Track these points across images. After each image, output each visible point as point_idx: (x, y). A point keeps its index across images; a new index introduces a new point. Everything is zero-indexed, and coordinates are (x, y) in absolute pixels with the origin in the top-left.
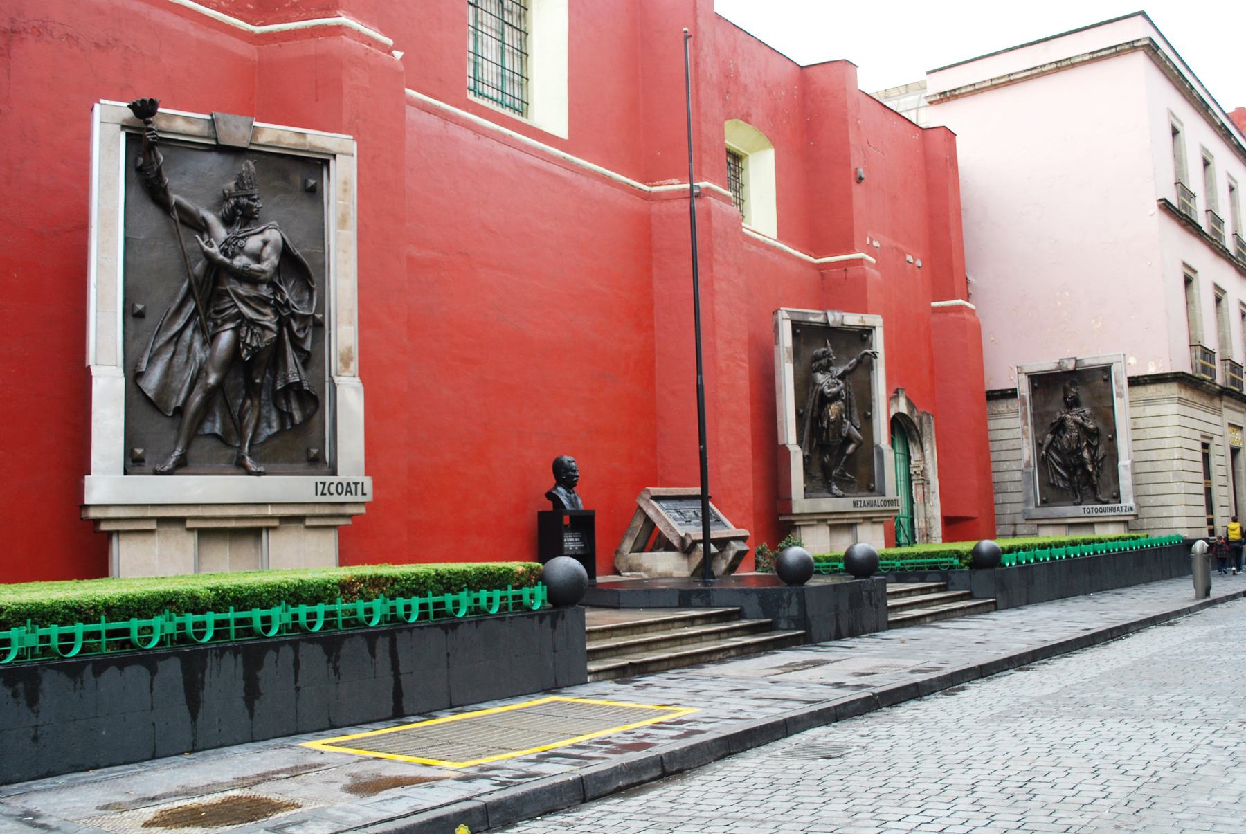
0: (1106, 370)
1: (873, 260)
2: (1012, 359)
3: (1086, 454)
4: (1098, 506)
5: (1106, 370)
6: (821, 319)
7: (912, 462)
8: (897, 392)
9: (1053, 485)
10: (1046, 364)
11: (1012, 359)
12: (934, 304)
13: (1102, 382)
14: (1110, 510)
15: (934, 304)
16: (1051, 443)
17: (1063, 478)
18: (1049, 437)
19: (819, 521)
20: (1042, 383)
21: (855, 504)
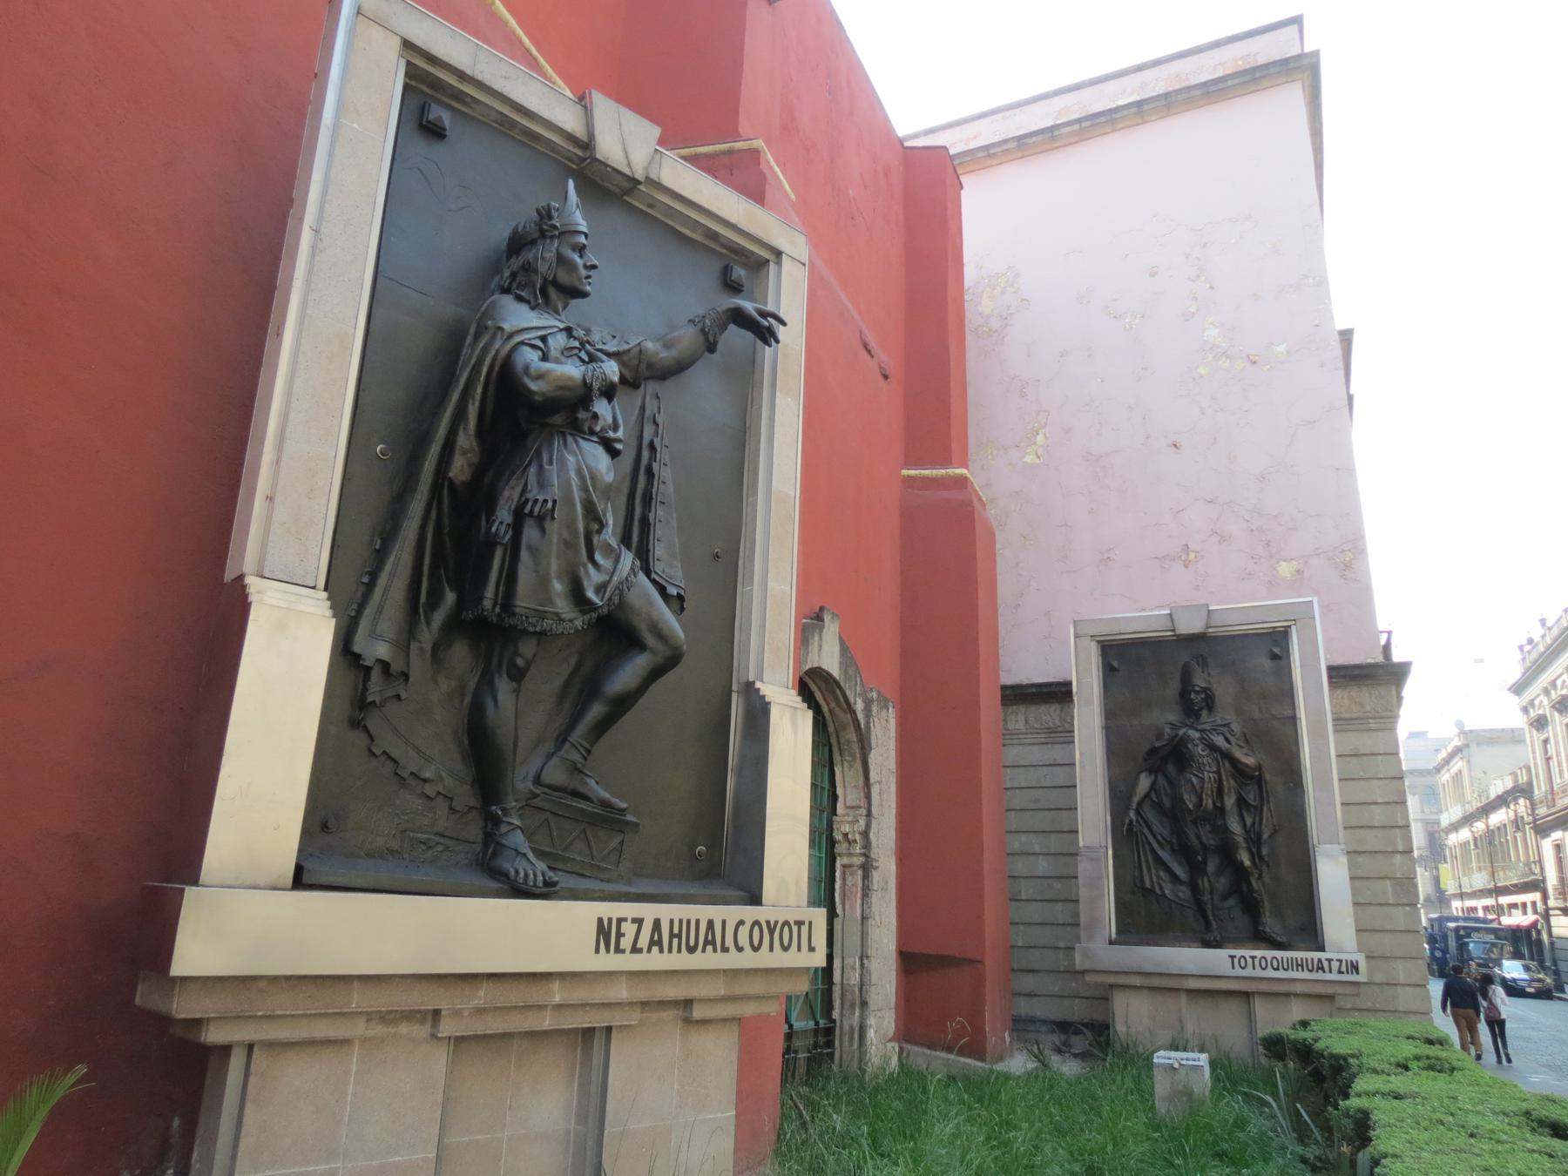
0: (1275, 643)
1: (793, 197)
2: (1048, 620)
3: (1235, 826)
4: (1269, 954)
5: (1275, 643)
6: (567, 117)
7: (840, 809)
8: (819, 618)
9: (1147, 892)
10: (1141, 608)
11: (1048, 620)
12: (905, 472)
13: (1267, 663)
14: (1300, 965)
15: (905, 472)
16: (1147, 795)
17: (1175, 878)
18: (1144, 783)
19: (386, 1018)
20: (1124, 658)
21: (606, 934)
